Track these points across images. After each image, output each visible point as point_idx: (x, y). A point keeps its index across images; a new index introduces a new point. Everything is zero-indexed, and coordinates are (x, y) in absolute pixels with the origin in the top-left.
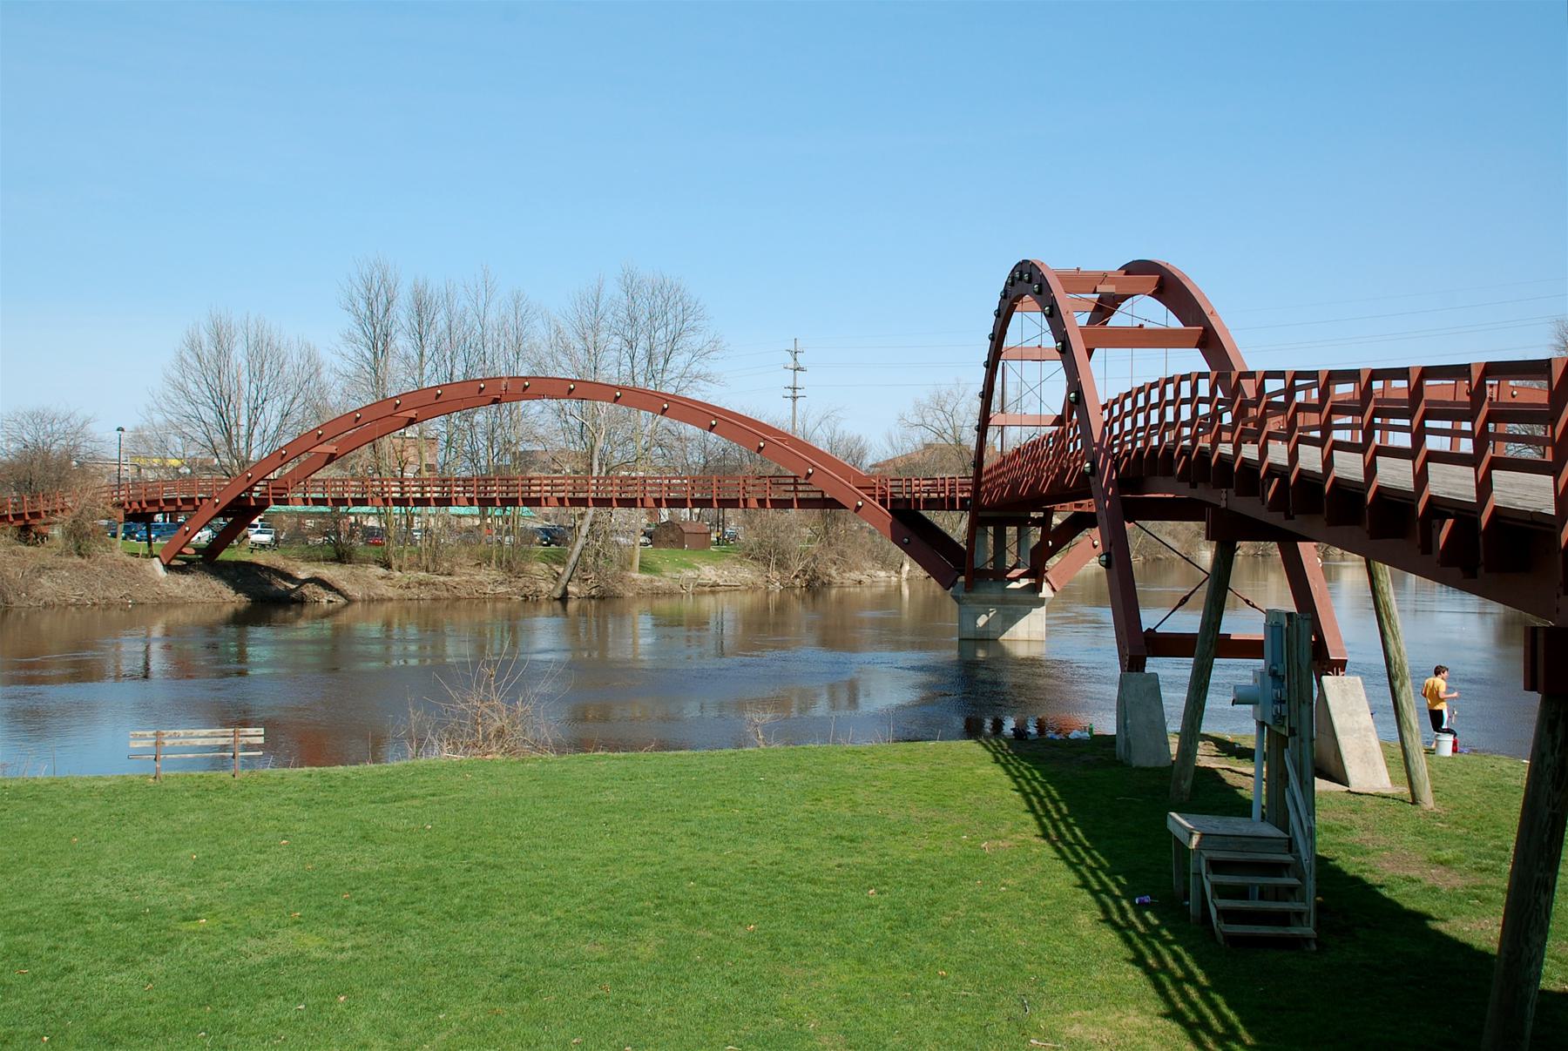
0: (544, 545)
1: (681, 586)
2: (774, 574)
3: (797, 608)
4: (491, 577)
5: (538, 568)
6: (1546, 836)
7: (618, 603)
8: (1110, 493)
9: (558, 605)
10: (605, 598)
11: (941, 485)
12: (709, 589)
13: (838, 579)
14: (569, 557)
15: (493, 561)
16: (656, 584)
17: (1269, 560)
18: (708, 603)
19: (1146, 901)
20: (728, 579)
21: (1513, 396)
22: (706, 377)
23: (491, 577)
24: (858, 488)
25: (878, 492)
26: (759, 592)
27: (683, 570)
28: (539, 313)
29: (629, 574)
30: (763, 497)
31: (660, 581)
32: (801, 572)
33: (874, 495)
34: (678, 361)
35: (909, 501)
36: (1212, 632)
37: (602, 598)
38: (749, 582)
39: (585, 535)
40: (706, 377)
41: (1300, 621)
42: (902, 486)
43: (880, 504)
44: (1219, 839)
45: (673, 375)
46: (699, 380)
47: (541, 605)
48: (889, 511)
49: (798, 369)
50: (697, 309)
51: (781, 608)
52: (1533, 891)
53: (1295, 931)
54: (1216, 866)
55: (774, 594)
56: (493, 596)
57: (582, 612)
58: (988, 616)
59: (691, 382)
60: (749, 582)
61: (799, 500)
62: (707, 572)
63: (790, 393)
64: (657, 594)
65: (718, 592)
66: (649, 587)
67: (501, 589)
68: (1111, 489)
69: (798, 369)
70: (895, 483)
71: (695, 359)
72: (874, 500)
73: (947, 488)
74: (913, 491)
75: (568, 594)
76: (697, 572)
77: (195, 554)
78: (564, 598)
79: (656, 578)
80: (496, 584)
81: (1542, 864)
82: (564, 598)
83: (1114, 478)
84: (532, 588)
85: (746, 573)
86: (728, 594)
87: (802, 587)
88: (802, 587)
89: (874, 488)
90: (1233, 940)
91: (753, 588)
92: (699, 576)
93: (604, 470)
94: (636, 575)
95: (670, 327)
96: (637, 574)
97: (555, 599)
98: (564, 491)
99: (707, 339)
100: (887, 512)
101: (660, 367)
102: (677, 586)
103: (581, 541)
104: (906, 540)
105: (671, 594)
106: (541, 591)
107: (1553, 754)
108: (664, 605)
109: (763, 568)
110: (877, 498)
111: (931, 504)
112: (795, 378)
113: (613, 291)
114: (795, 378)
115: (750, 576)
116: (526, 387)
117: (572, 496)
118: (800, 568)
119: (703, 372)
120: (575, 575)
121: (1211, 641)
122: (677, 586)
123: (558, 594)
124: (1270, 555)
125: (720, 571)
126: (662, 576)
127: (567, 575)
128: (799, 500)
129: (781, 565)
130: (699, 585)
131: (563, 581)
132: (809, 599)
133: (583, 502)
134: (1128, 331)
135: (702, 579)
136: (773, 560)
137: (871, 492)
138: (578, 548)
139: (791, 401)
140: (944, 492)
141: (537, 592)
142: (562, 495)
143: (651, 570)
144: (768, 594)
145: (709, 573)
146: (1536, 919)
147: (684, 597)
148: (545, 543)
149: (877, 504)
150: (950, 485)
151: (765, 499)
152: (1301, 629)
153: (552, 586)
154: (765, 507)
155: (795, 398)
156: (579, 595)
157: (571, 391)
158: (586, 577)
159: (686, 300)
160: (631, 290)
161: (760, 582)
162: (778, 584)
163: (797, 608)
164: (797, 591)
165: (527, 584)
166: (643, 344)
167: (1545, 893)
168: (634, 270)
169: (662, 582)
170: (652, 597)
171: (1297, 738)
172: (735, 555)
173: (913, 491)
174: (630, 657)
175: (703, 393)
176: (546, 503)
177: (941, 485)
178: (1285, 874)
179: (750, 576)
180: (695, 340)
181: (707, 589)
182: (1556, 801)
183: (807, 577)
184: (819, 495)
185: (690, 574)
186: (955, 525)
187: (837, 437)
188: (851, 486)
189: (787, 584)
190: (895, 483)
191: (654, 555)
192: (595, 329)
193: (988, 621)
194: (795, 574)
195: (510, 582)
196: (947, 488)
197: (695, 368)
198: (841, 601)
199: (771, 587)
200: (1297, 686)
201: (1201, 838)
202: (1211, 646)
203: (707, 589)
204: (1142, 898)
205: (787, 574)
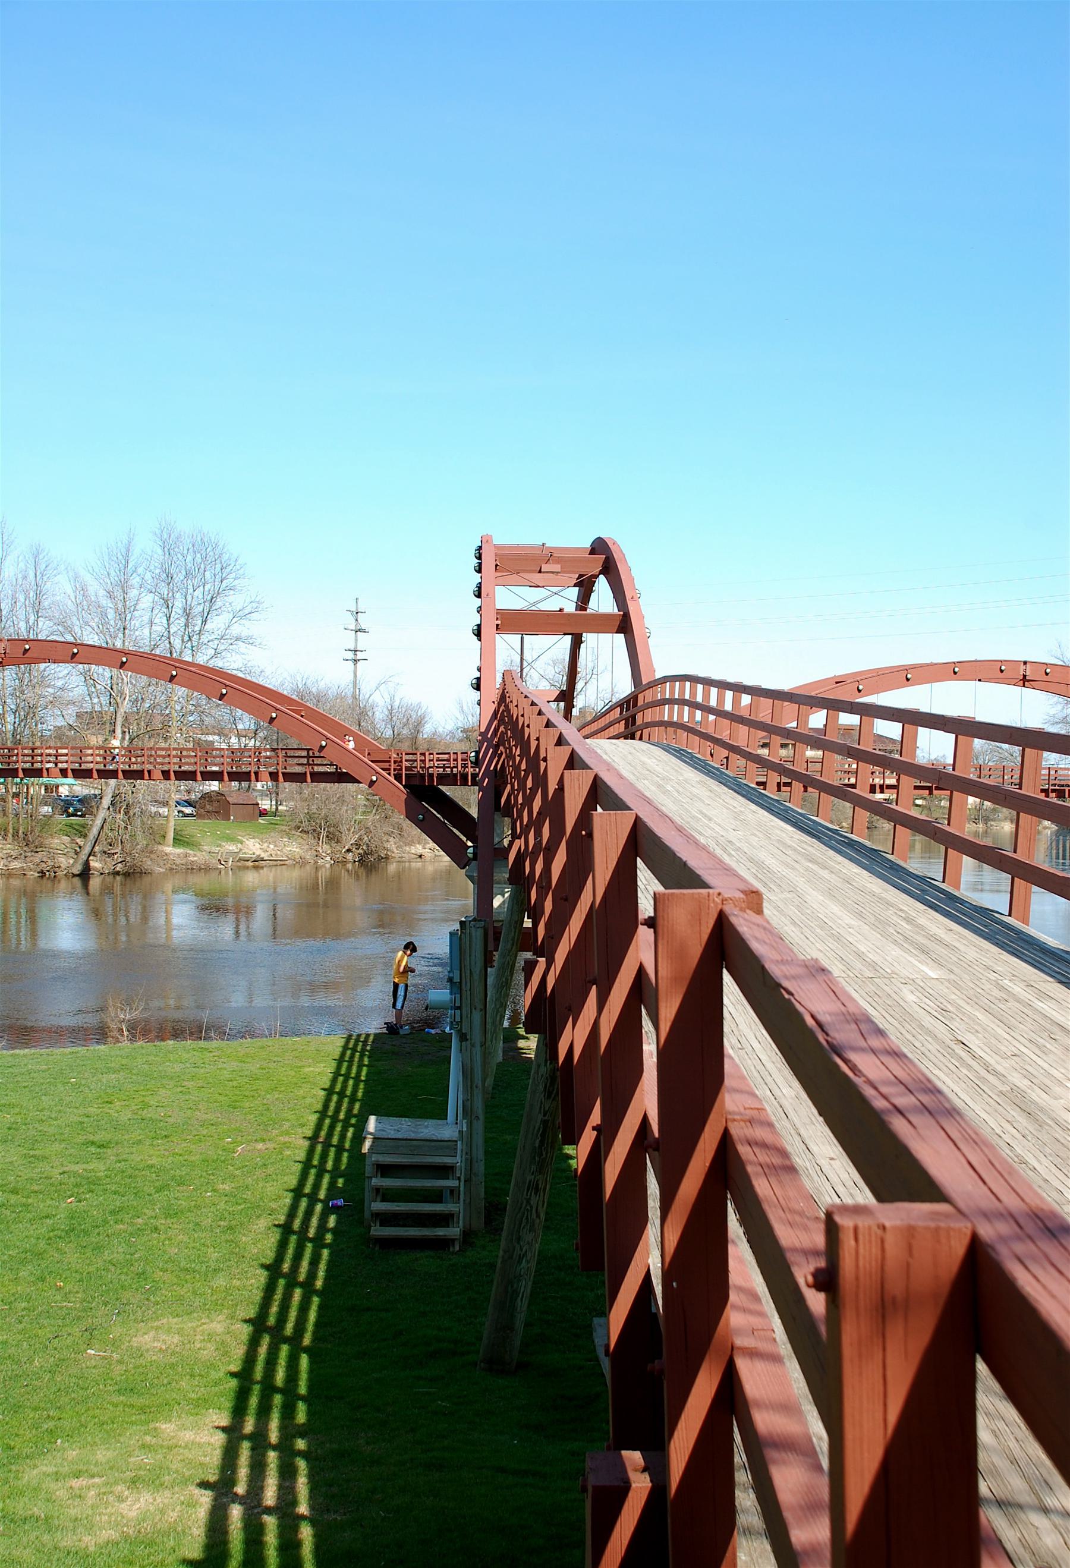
0: (80, 816)
1: (219, 860)
2: (325, 848)
3: (348, 883)
4: (5, 852)
5: (59, 842)
6: (538, 1141)
7: (147, 879)
8: (485, 785)
9: (77, 880)
10: (131, 874)
11: (454, 760)
12: (252, 864)
13: (396, 853)
14: (89, 830)
15: (10, 835)
16: (191, 859)
17: (875, 832)
18: (251, 878)
19: (339, 1204)
20: (273, 852)
21: (1047, 674)
22: (247, 640)
23: (5, 852)
24: (372, 761)
25: (393, 766)
26: (308, 867)
27: (223, 844)
28: (62, 567)
29: (160, 847)
30: (303, 771)
31: (195, 856)
32: (354, 846)
33: (389, 769)
34: (216, 624)
35: (422, 776)
36: (513, 930)
37: (127, 875)
38: (297, 857)
39: (106, 807)
40: (247, 640)
41: (473, 930)
42: (416, 761)
43: (395, 779)
44: (392, 1143)
45: (213, 637)
46: (240, 643)
47: (59, 881)
48: (404, 787)
49: (359, 630)
50: (238, 567)
51: (333, 883)
52: (525, 1193)
53: (440, 1232)
54: (384, 1170)
55: (324, 870)
56: (7, 872)
57: (107, 890)
58: (504, 897)
59: (231, 644)
60: (297, 857)
61: (313, 774)
62: (251, 847)
63: (350, 655)
64: (191, 869)
65: (262, 868)
66: (183, 862)
67: (16, 865)
68: (487, 780)
69: (359, 630)
70: (410, 757)
71: (235, 620)
72: (389, 774)
73: (460, 762)
74: (427, 766)
75: (90, 870)
76: (239, 845)
77: (353, 749)
78: (85, 874)
79: (191, 852)
80: (9, 859)
81: (534, 1168)
82: (85, 874)
83: (492, 769)
84: (50, 863)
85: (294, 848)
86: (274, 869)
87: (355, 861)
88: (355, 861)
89: (389, 762)
90: (387, 1244)
91: (301, 863)
92: (241, 850)
93: (127, 737)
94: (168, 849)
95: (207, 587)
96: (171, 849)
97: (74, 875)
98: (92, 762)
99: (248, 600)
100: (401, 787)
101: (197, 629)
102: (215, 861)
103: (102, 814)
104: (421, 816)
105: (206, 869)
106: (59, 867)
107: (546, 1065)
108: (200, 881)
109: (313, 842)
110: (392, 772)
111: (444, 779)
112: (356, 640)
113: (146, 546)
114: (356, 640)
115: (297, 850)
116: (26, 651)
117: (78, 768)
118: (353, 841)
119: (243, 635)
120: (97, 849)
121: (513, 939)
122: (215, 861)
123: (77, 869)
124: (876, 827)
125: (266, 845)
126: (199, 850)
127: (87, 850)
128: (313, 774)
129: (333, 838)
130: (240, 859)
131: (83, 857)
132: (362, 872)
133: (113, 774)
134: (548, 615)
135: (245, 853)
136: (324, 834)
137: (386, 765)
138: (99, 822)
139: (351, 663)
140: (457, 767)
141: (55, 868)
142: (65, 766)
143: (188, 843)
144: (317, 869)
145: (253, 847)
146: (527, 1218)
147: (223, 872)
148: (79, 813)
149: (392, 779)
150: (462, 760)
151: (277, 773)
152: (474, 937)
153: (71, 861)
154: (306, 782)
155: (356, 661)
156: (102, 871)
157: (74, 655)
158: (112, 851)
159: (225, 557)
160: (168, 545)
161: (309, 856)
162: (328, 858)
163: (348, 883)
164: (350, 866)
165: (44, 860)
166: (179, 604)
167: (536, 1194)
168: (172, 524)
169: (197, 857)
170: (186, 873)
171: (468, 1042)
172: (284, 828)
173: (427, 766)
174: (163, 941)
175: (243, 656)
176: (48, 774)
177: (454, 760)
178: (451, 1177)
179: (297, 850)
180: (236, 600)
181: (250, 864)
182: (547, 1109)
183: (361, 851)
184: (332, 769)
185: (232, 848)
186: (469, 799)
187: (396, 704)
188: (366, 760)
189: (338, 858)
190: (410, 757)
191: (196, 828)
192: (124, 587)
193: (504, 902)
194: (347, 848)
195: (26, 857)
196: (460, 762)
197: (236, 630)
198: (399, 875)
199: (320, 861)
200: (469, 992)
201: (373, 1142)
202: (513, 945)
203: (250, 864)
204: (335, 1202)
205: (338, 848)
